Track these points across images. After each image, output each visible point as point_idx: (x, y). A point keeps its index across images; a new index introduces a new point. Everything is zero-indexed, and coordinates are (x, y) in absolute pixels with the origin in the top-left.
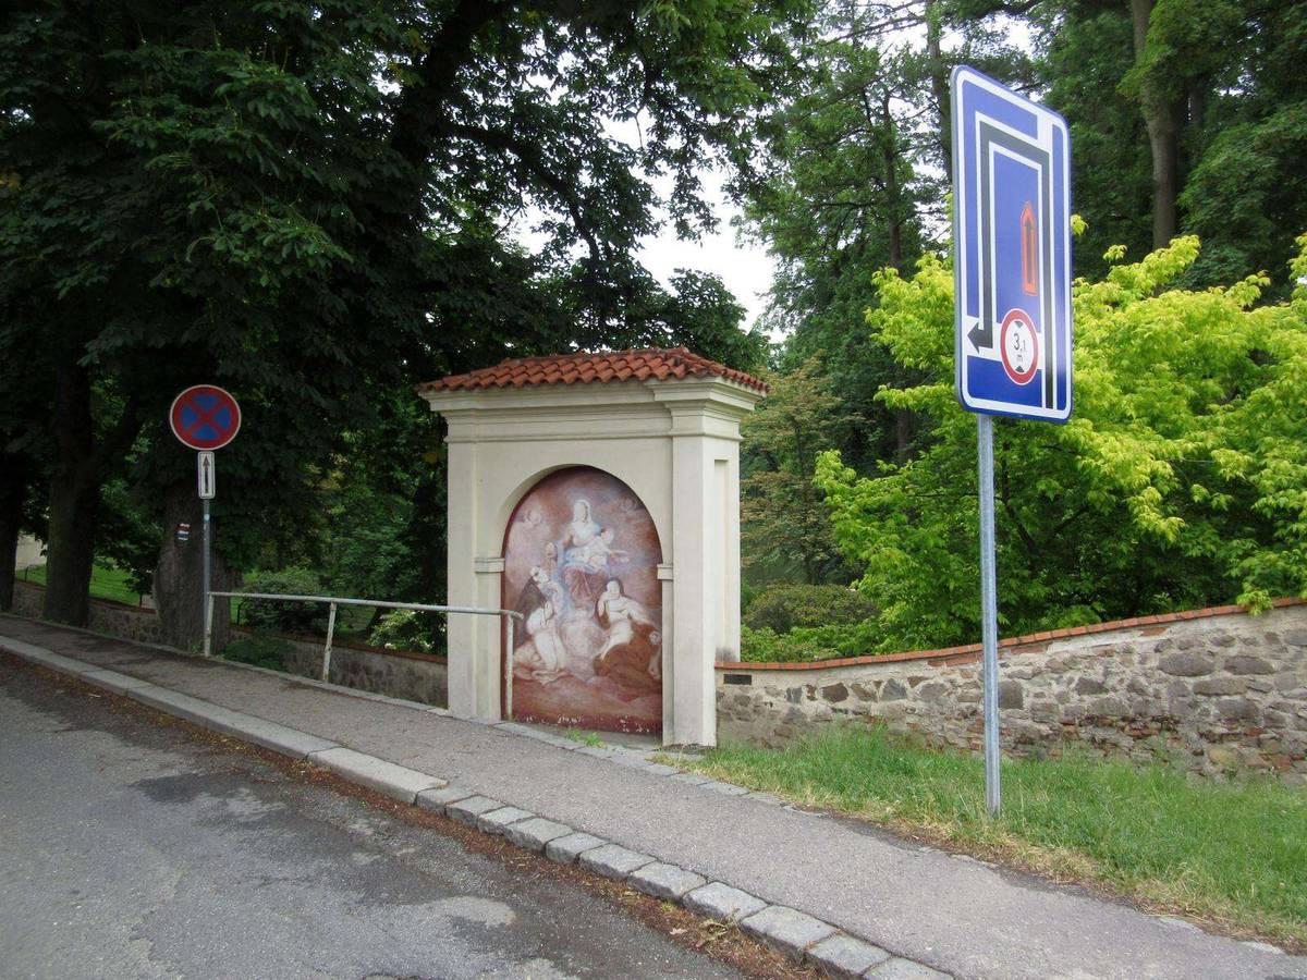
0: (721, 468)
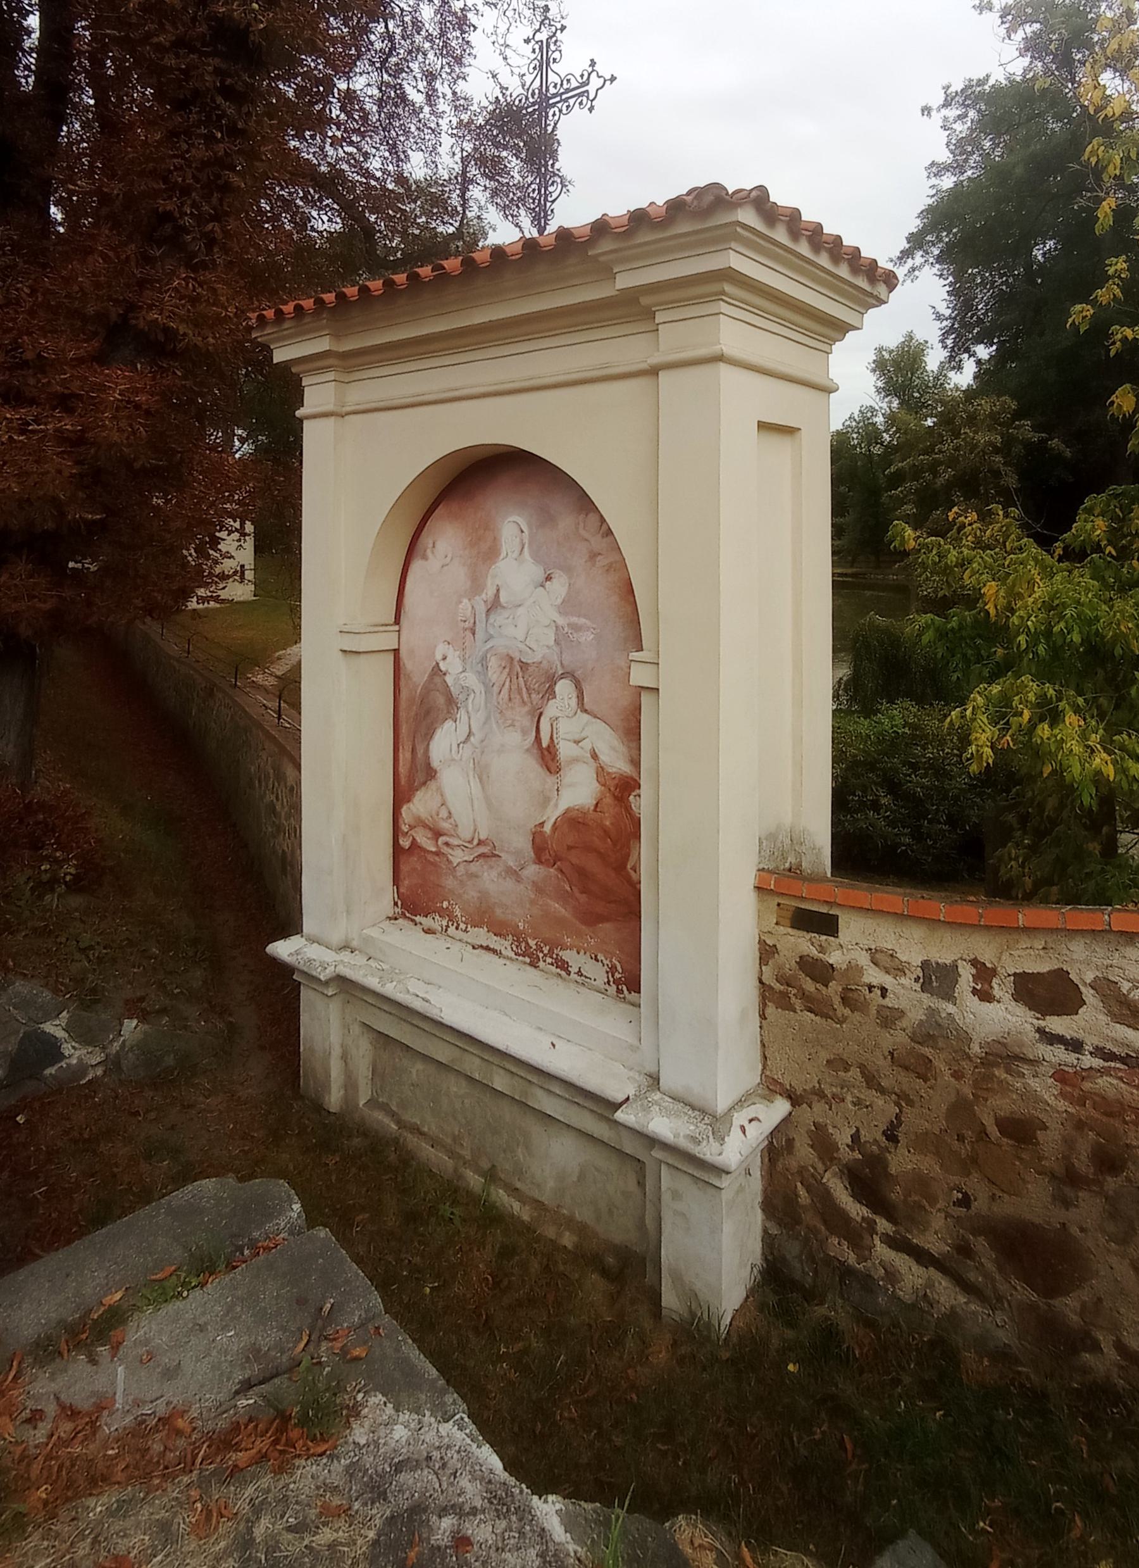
0: (780, 446)
